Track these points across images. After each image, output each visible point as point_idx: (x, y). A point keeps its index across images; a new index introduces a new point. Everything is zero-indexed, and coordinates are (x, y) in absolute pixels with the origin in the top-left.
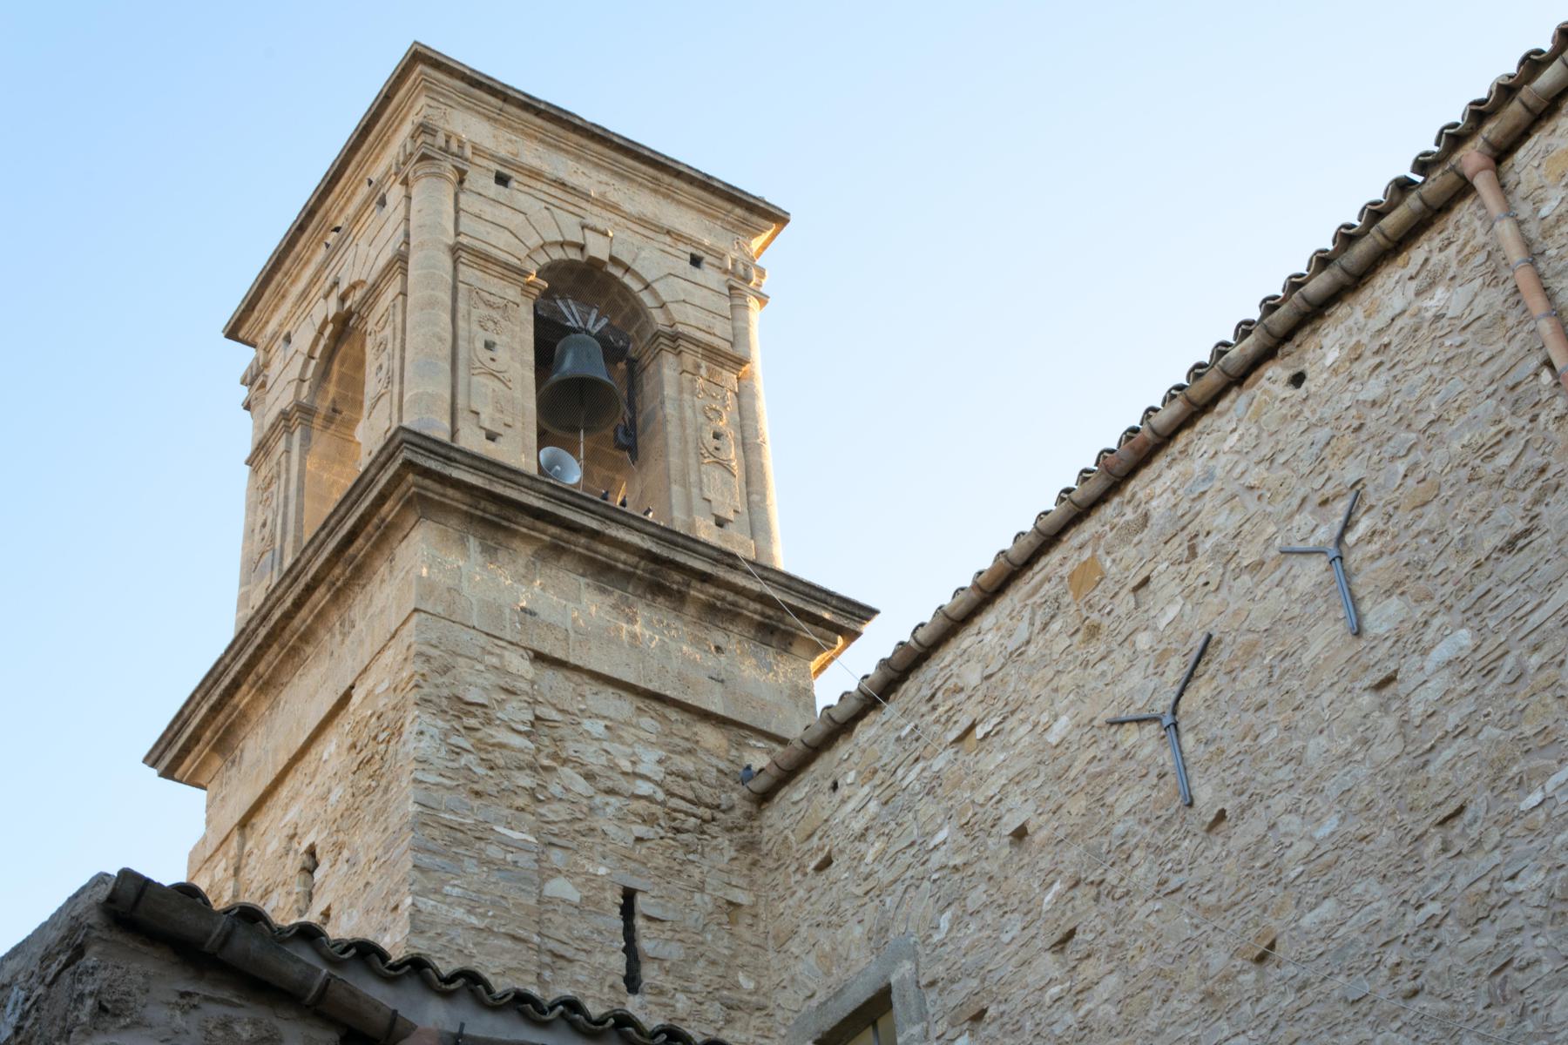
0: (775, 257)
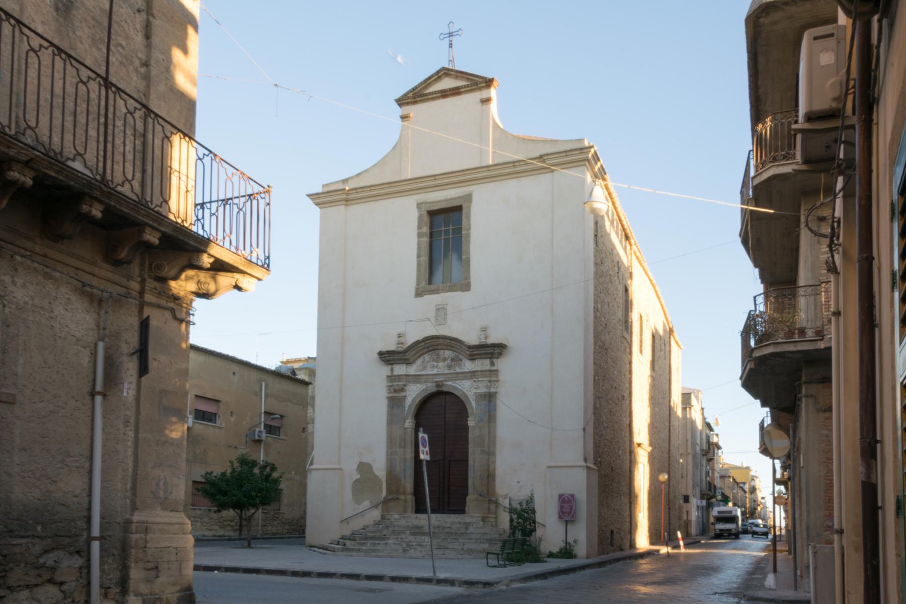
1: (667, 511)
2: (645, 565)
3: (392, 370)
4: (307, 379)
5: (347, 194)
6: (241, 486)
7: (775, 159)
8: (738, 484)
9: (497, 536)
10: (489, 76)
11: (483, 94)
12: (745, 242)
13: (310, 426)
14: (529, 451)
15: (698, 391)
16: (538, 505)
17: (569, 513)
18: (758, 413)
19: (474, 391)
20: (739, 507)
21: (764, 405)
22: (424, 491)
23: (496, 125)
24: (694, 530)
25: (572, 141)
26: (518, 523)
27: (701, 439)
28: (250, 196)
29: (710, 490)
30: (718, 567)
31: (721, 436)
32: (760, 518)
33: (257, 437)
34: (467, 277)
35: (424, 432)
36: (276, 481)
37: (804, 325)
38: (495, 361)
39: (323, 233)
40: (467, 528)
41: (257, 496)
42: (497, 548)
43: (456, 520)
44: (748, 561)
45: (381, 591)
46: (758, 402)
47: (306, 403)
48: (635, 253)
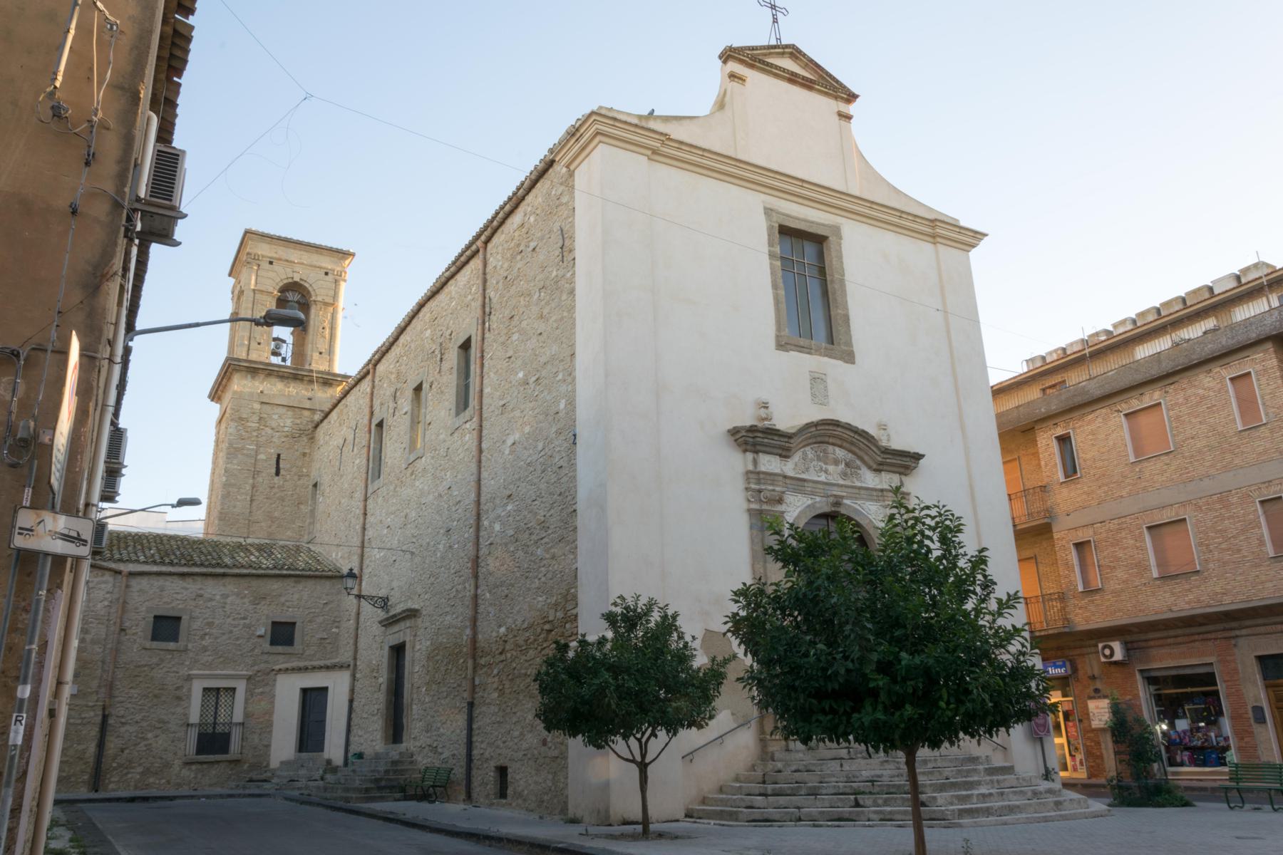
0: (352, 269)
3: (755, 462)
10: (855, 90)
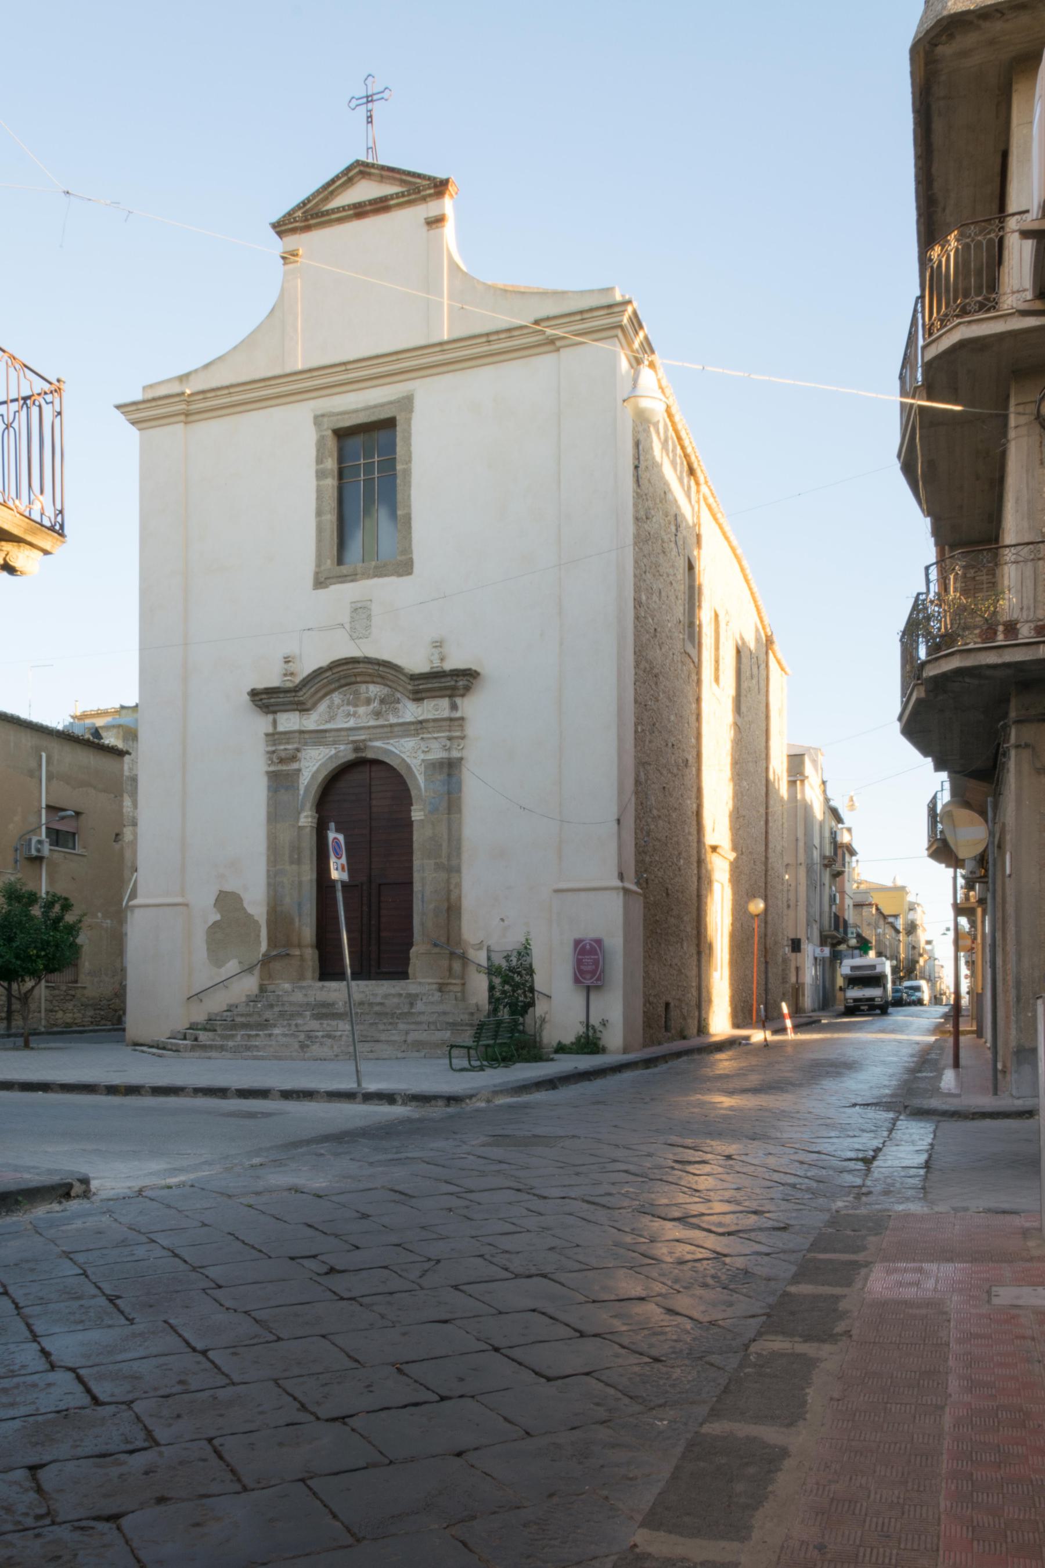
1: (763, 968)
2: (724, 1063)
3: (275, 723)
4: (120, 745)
5: (188, 403)
6: (10, 940)
7: (964, 312)
8: (885, 917)
9: (466, 1017)
10: (441, 175)
11: (431, 209)
12: (908, 469)
13: (128, 833)
14: (520, 868)
15: (816, 749)
16: (538, 960)
17: (593, 973)
18: (928, 782)
19: (422, 756)
20: (887, 958)
21: (939, 767)
22: (340, 940)
23: (454, 267)
24: (808, 1001)
25: (591, 291)
26: (504, 992)
27: (822, 837)
28: (25, 399)
29: (837, 928)
30: (855, 1062)
31: (856, 832)
32: (923, 978)
33: (34, 853)
34: (407, 549)
35: (338, 830)
36: (72, 930)
37: (1015, 616)
38: (458, 701)
39: (145, 475)
40: (412, 1005)
41: (38, 956)
42: (467, 1038)
43: (393, 991)
44: (906, 1051)
45: (266, 1115)
46: (929, 762)
47: (122, 787)
48: (705, 499)
